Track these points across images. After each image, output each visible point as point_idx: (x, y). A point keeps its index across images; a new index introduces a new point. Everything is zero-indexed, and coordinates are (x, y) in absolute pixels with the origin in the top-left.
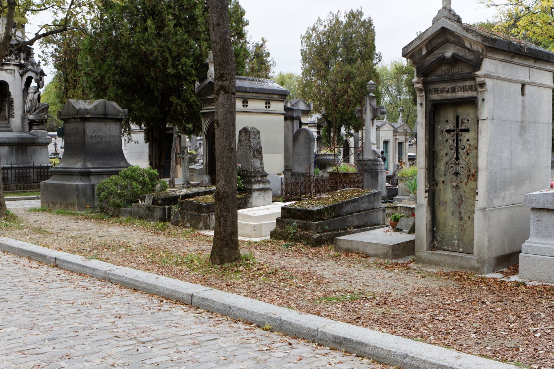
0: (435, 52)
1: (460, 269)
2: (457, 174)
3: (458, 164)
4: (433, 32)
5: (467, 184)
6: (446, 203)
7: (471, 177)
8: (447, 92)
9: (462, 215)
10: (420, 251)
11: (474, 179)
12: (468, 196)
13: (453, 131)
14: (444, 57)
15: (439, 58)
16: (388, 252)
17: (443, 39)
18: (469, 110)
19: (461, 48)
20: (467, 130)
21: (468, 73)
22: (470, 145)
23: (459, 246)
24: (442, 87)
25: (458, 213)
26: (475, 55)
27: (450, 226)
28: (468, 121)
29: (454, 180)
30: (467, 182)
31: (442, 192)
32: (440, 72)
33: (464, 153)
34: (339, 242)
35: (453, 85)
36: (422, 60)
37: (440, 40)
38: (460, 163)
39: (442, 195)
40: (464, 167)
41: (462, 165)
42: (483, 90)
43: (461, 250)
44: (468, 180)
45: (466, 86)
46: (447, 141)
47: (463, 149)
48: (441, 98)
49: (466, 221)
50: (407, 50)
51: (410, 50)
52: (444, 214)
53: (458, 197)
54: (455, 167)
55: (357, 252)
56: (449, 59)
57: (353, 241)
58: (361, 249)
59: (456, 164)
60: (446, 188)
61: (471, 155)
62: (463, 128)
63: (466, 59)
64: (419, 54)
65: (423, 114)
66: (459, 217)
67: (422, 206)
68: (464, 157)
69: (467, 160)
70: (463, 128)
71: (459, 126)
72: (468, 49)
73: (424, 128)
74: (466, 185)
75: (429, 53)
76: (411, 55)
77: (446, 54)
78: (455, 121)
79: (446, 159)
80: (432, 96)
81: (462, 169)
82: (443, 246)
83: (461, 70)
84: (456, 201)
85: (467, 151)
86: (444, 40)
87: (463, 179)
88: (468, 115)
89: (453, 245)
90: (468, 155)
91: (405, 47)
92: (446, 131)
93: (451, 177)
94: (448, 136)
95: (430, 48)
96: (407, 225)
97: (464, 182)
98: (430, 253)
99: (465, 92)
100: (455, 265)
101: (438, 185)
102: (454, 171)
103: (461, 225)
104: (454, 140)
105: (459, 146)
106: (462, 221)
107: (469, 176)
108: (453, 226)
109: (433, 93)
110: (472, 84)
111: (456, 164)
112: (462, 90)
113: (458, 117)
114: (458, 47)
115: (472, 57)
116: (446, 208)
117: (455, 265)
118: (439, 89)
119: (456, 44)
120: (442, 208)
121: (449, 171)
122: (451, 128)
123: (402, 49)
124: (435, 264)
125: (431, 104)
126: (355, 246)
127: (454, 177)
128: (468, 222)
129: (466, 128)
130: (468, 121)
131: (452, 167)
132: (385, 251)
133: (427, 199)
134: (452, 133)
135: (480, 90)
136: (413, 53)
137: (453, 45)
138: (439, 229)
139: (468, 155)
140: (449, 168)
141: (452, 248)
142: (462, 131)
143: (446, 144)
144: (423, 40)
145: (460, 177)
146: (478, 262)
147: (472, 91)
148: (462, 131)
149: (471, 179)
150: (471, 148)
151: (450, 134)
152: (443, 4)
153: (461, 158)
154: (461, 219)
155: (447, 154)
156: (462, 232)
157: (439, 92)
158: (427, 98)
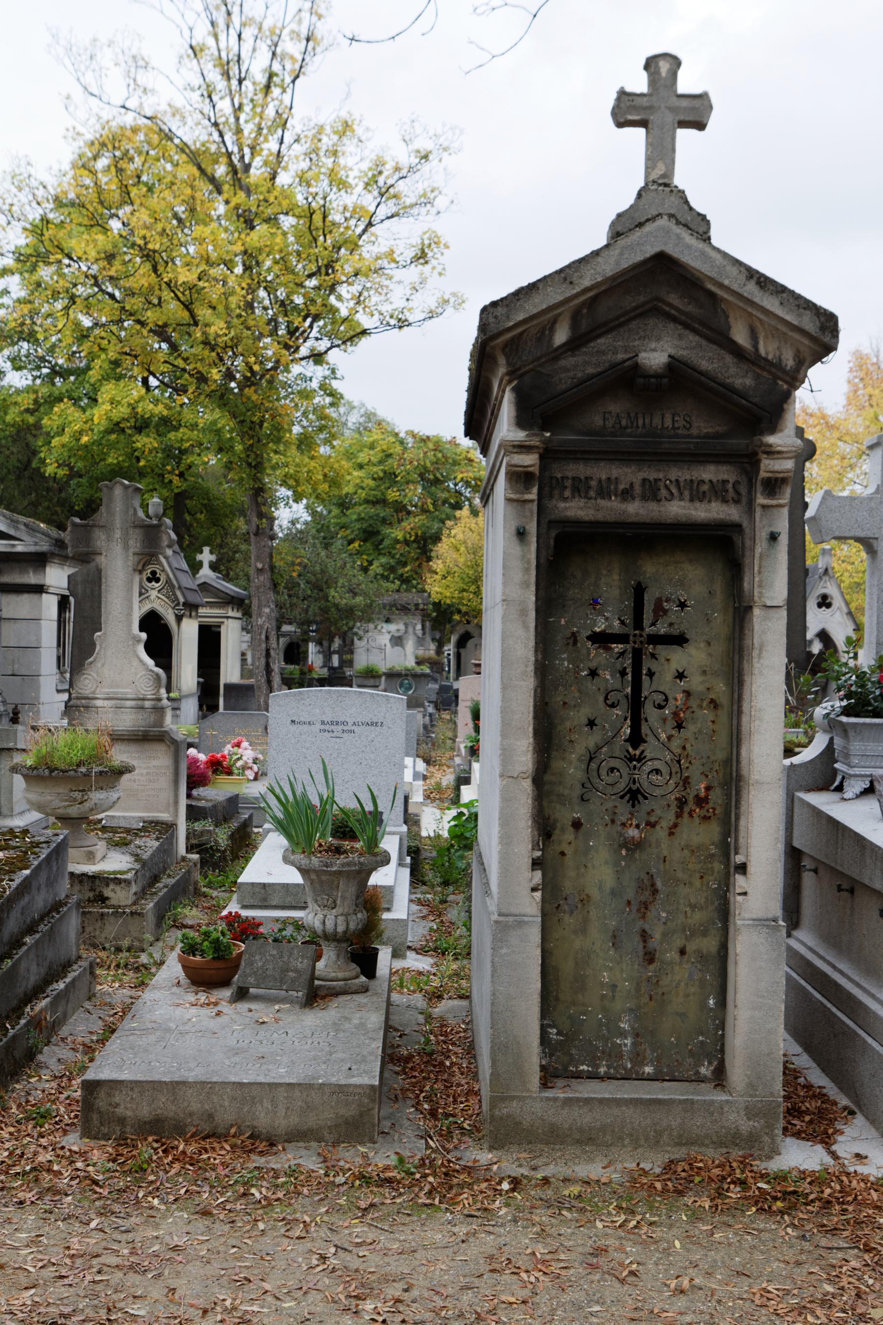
0: (601, 341)
1: (684, 1150)
2: (634, 795)
3: (639, 760)
4: (625, 265)
5: (677, 831)
6: (585, 901)
7: (691, 805)
8: (627, 495)
9: (653, 943)
10: (513, 1098)
11: (703, 813)
12: (680, 875)
13: (621, 638)
14: (636, 366)
15: (614, 366)
16: (361, 1115)
17: (642, 299)
18: (687, 567)
19: (704, 343)
20: (680, 640)
21: (707, 436)
22: (688, 694)
23: (638, 1058)
24: (604, 477)
25: (637, 939)
26: (757, 377)
27: (602, 984)
28: (683, 605)
29: (623, 819)
30: (675, 825)
31: (569, 860)
32: (598, 421)
33: (664, 720)
34: (109, 1095)
35: (652, 475)
36: (541, 365)
37: (630, 302)
38: (648, 754)
39: (572, 874)
40: (665, 770)
41: (657, 764)
42: (774, 502)
43: (648, 1069)
44: (679, 815)
45: (703, 482)
46: (593, 673)
47: (660, 707)
48: (600, 516)
49: (671, 963)
50: (508, 318)
51: (521, 317)
52: (578, 943)
53: (640, 880)
54: (625, 771)
55: (207, 1128)
56: (657, 376)
57: (184, 1083)
58: (226, 1115)
59: (631, 759)
60: (587, 850)
61: (691, 729)
62: (662, 631)
63: (723, 385)
64: (539, 340)
65: (527, 570)
66: (641, 953)
67: (520, 924)
68: (663, 736)
69: (675, 745)
70: (662, 628)
71: (646, 623)
72: (737, 352)
73: (532, 625)
74: (671, 834)
75: (574, 345)
76: (513, 339)
77: (643, 355)
78: (629, 603)
79: (592, 740)
80: (562, 505)
81: (654, 777)
82: (571, 1060)
83: (681, 423)
84: (630, 894)
85: (675, 714)
86: (644, 304)
87: (658, 812)
88: (681, 583)
89: (615, 1054)
90: (679, 726)
91: (494, 304)
92: (589, 638)
93: (610, 805)
94: (596, 656)
95: (584, 325)
96: (285, 970)
97: (665, 824)
98: (556, 1099)
99: (698, 504)
100: (659, 1133)
101: (554, 837)
102: (622, 785)
103: (649, 980)
104: (623, 673)
105: (645, 693)
106: (652, 967)
107: (682, 803)
108: (614, 987)
109: (567, 493)
110: (725, 477)
111: (631, 759)
112: (687, 493)
113: (639, 591)
114: (693, 338)
115: (749, 382)
116: (586, 921)
117: (659, 1133)
118: (594, 483)
119: (686, 326)
120: (568, 919)
121: (601, 785)
122: (610, 626)
123: (484, 310)
124: (578, 1142)
125: (553, 533)
126: (195, 1106)
127: (623, 809)
128: (677, 968)
129: (675, 631)
130: (683, 605)
131: (612, 770)
132: (351, 1111)
133: (538, 895)
134: (617, 648)
135: (761, 500)
136: (521, 334)
137: (671, 325)
138: (557, 999)
139: (679, 726)
140: (603, 772)
141: (609, 1067)
142: (656, 639)
143: (591, 686)
144: (578, 289)
145: (645, 806)
146: (751, 1113)
147: (725, 501)
148: (656, 639)
149: (691, 815)
150: (694, 703)
151: (608, 649)
152: (648, 169)
153: (651, 739)
154: (650, 957)
155: (591, 723)
156: (652, 1004)
157: (592, 494)
158: (541, 510)
